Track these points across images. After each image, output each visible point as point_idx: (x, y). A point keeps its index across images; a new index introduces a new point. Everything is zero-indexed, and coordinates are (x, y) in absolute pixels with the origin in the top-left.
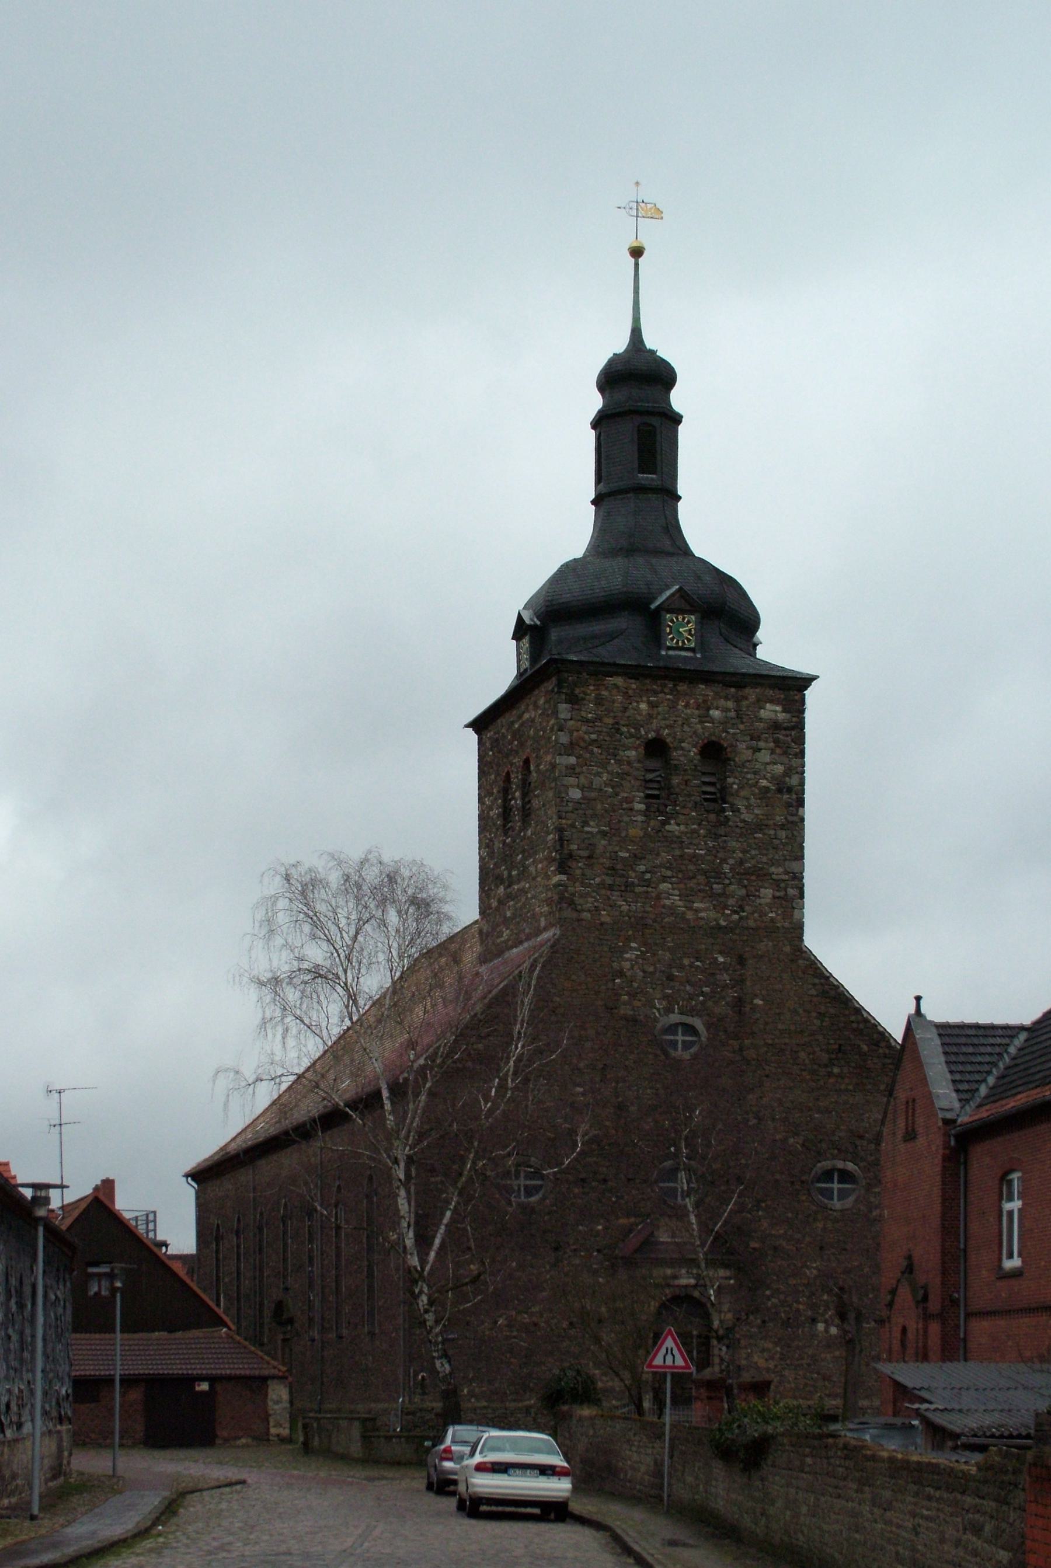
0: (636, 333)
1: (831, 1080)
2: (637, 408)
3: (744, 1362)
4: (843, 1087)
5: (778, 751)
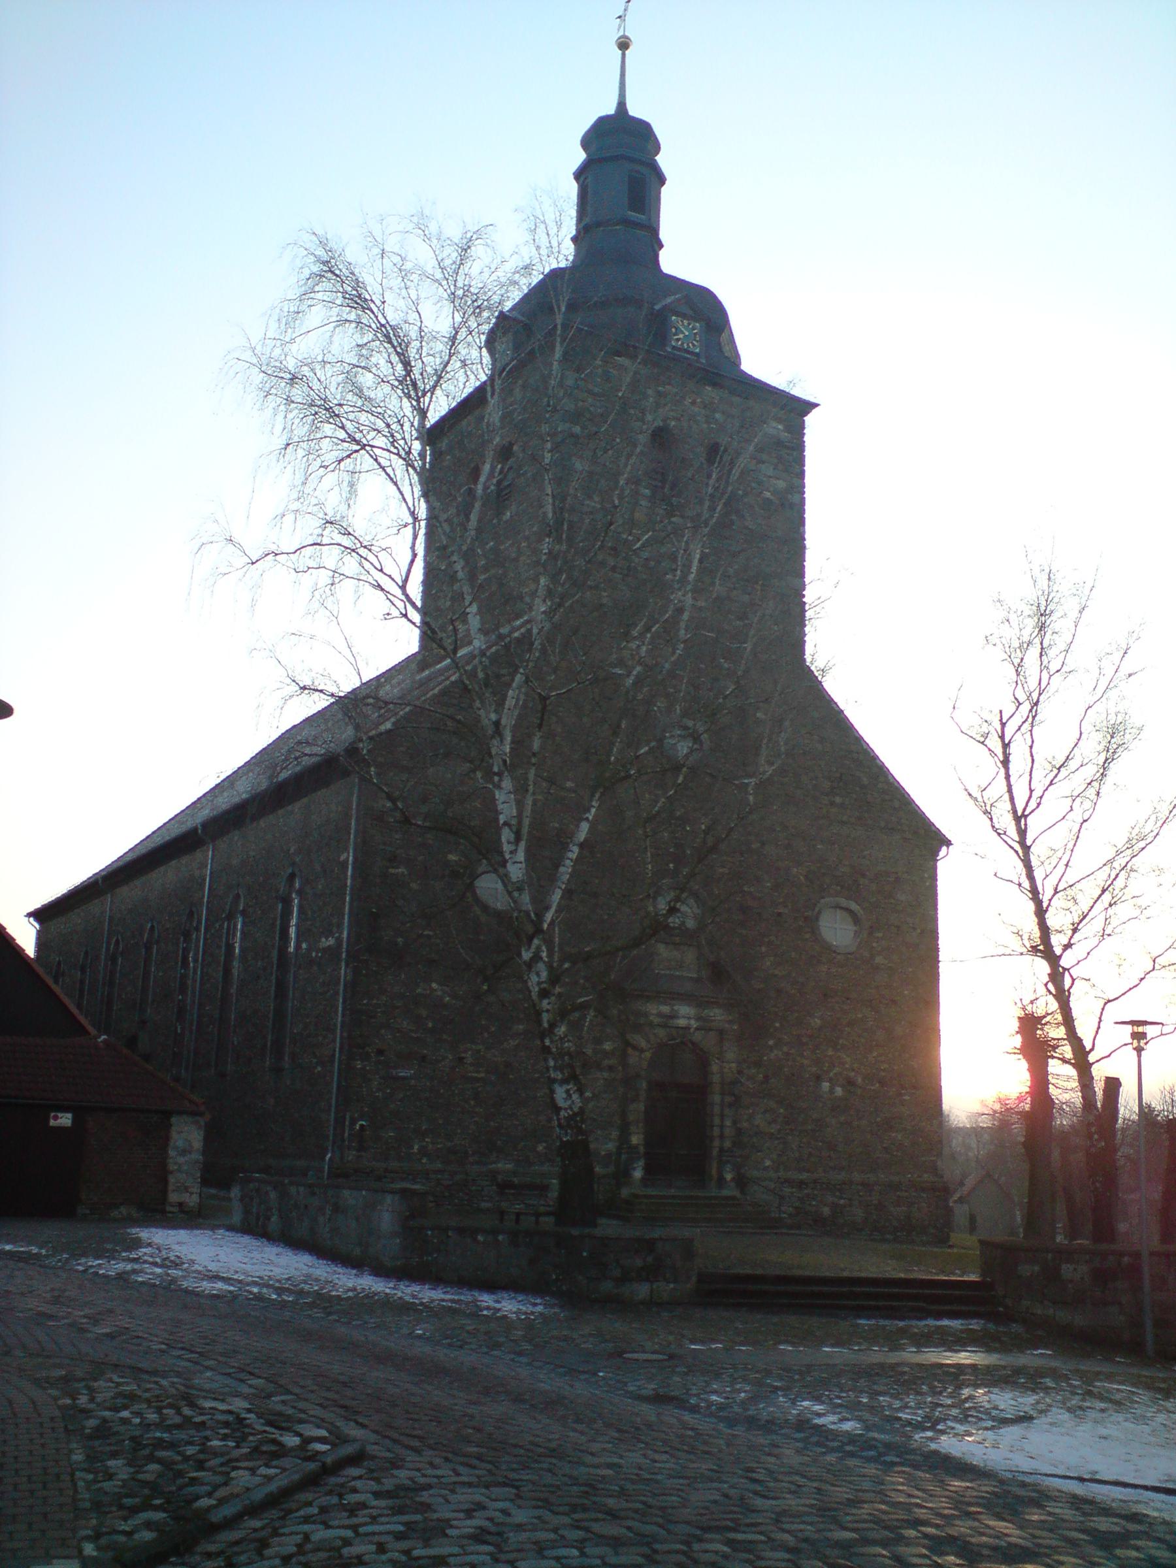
0: (622, 105)
1: (834, 810)
2: (621, 167)
3: (745, 1125)
4: (845, 818)
5: (780, 467)
